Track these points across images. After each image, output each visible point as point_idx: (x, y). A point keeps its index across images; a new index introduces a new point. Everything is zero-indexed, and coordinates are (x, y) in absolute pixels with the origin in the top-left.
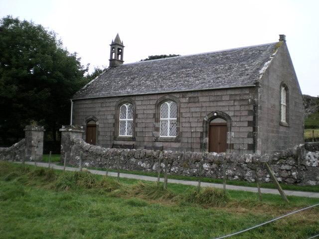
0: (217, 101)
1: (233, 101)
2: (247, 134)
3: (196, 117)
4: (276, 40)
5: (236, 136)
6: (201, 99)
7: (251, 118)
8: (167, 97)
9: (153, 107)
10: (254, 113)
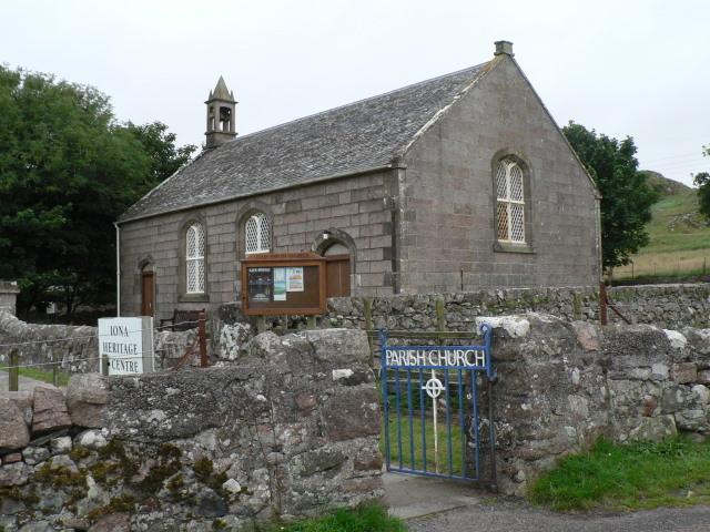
0: (331, 207)
1: (357, 205)
2: (381, 277)
3: (298, 245)
4: (488, 55)
5: (366, 284)
6: (307, 204)
7: (387, 241)
8: (252, 205)
9: (232, 228)
10: (392, 228)
